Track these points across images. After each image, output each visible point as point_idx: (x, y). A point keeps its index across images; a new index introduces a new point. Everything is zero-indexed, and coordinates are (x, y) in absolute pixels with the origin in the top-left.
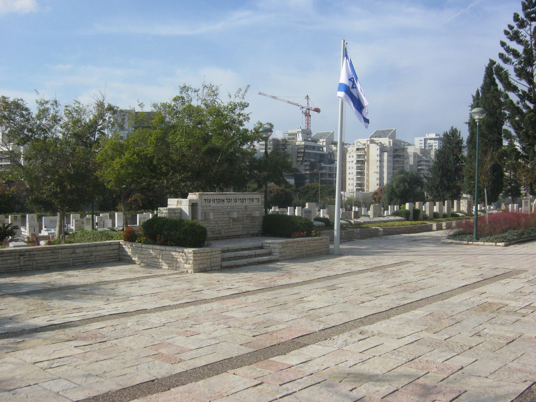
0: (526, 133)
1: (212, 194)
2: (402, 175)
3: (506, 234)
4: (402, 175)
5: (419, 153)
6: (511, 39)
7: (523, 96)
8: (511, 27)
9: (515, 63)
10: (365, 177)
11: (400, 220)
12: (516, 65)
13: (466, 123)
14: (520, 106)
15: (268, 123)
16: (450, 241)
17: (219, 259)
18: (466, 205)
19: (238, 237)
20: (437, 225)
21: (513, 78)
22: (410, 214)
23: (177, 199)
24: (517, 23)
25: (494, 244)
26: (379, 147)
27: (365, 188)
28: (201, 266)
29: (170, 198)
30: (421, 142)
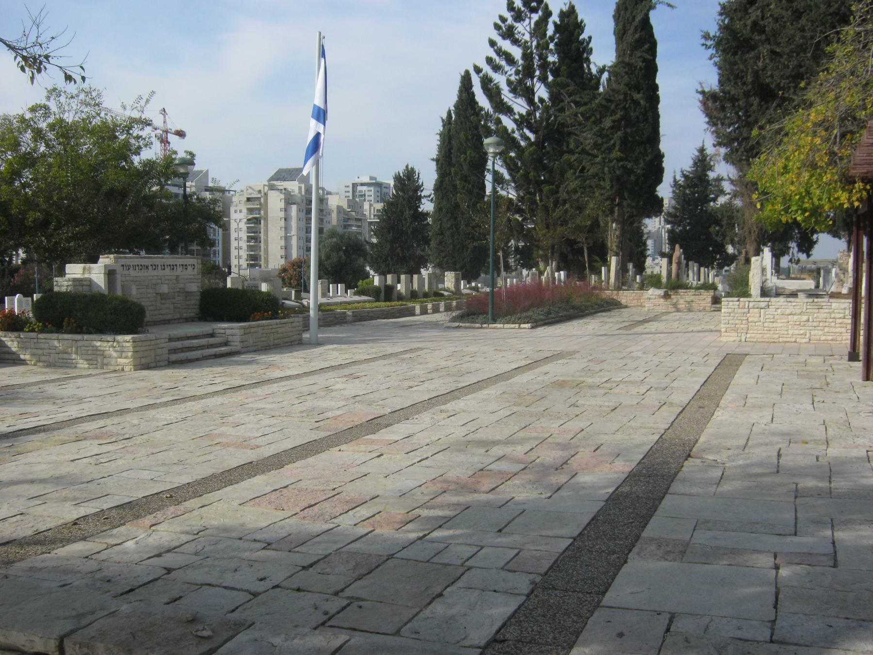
0: (526, 176)
1: (131, 258)
2: (335, 240)
3: (530, 313)
4: (335, 240)
5: (345, 206)
6: (504, 36)
7: (522, 122)
8: (503, 19)
9: (509, 73)
10: (262, 244)
11: (369, 302)
12: (510, 75)
13: (433, 160)
14: (517, 135)
15: (186, 152)
16: (457, 324)
17: (165, 351)
18: (453, 280)
19: (167, 322)
20: (421, 308)
21: (507, 96)
22: (381, 292)
23: (83, 265)
24: (512, 13)
25: (517, 325)
26: (283, 196)
27: (262, 263)
28: (143, 361)
29: (70, 263)
30: (347, 189)
